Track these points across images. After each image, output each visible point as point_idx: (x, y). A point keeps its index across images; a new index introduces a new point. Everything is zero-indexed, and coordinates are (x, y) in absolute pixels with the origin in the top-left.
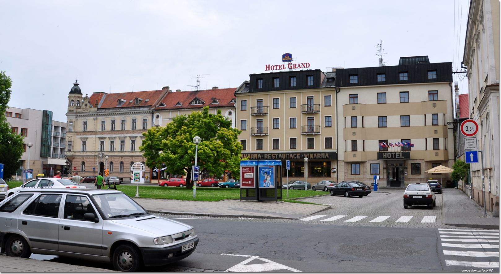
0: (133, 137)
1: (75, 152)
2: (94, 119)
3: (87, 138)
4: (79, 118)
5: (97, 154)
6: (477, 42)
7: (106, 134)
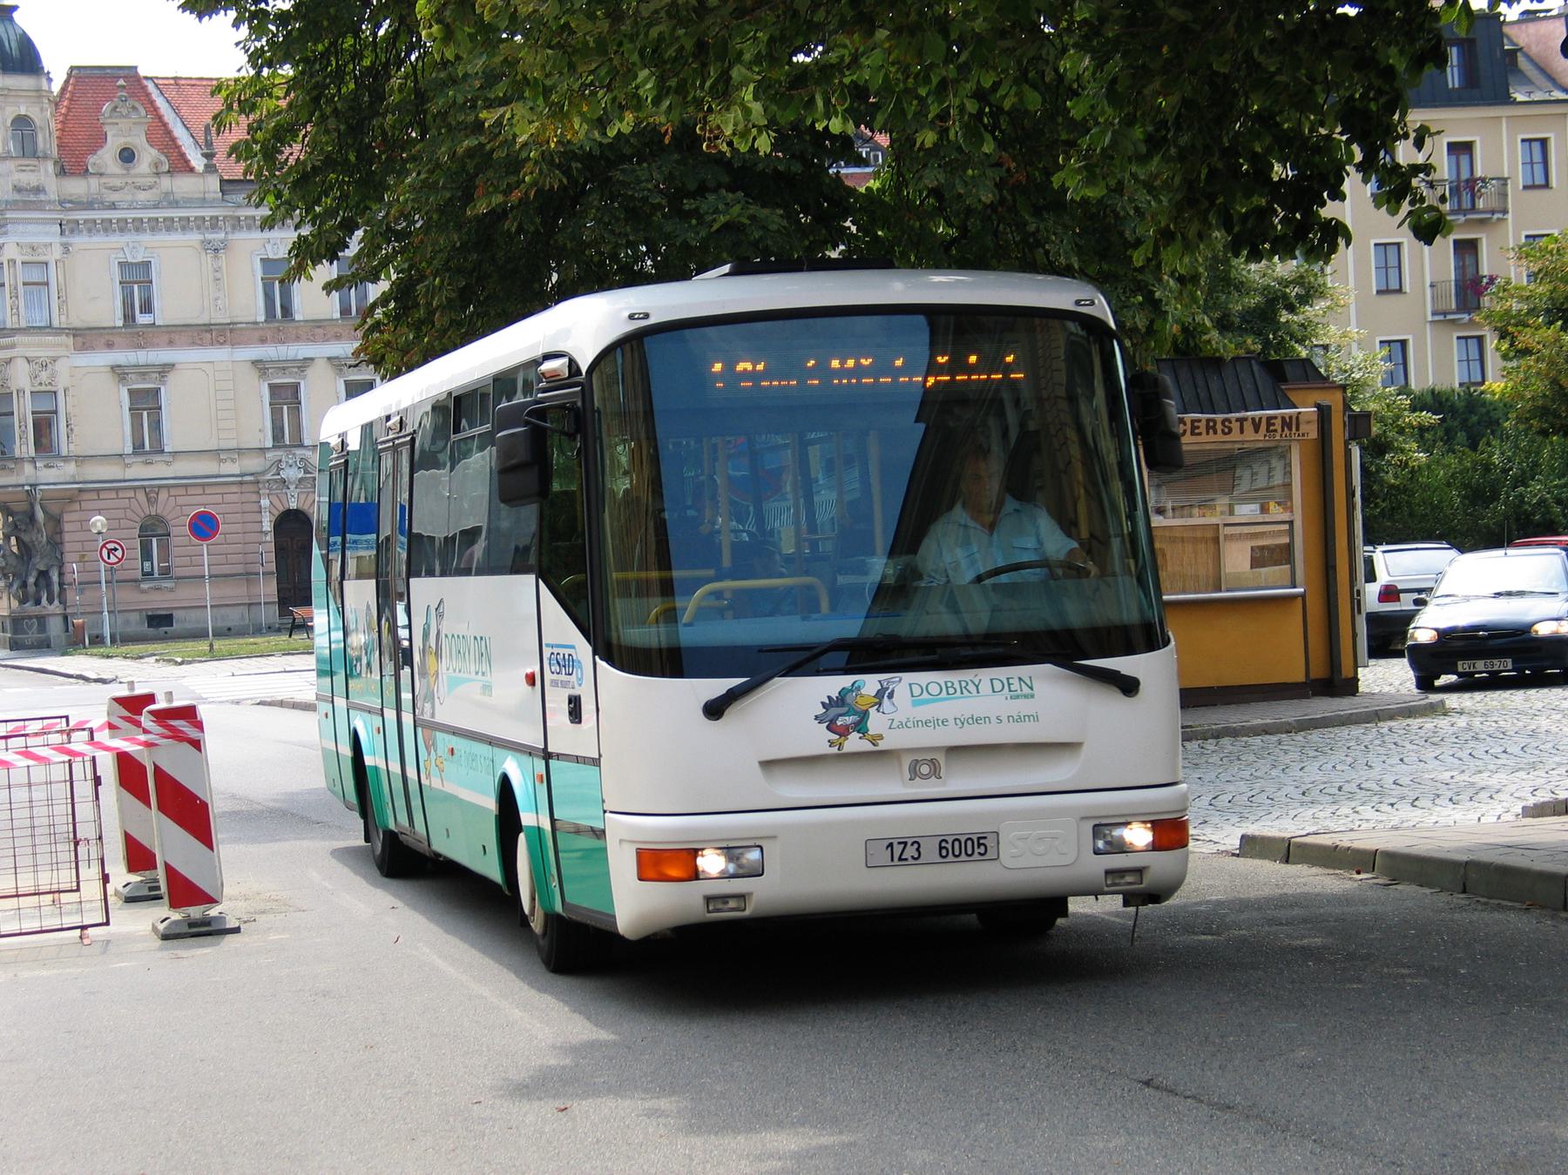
0: (283, 366)
1: (81, 459)
2: (207, 246)
3: (165, 369)
4: (79, 241)
5: (253, 464)
6: (1186, 478)
7: (312, 339)
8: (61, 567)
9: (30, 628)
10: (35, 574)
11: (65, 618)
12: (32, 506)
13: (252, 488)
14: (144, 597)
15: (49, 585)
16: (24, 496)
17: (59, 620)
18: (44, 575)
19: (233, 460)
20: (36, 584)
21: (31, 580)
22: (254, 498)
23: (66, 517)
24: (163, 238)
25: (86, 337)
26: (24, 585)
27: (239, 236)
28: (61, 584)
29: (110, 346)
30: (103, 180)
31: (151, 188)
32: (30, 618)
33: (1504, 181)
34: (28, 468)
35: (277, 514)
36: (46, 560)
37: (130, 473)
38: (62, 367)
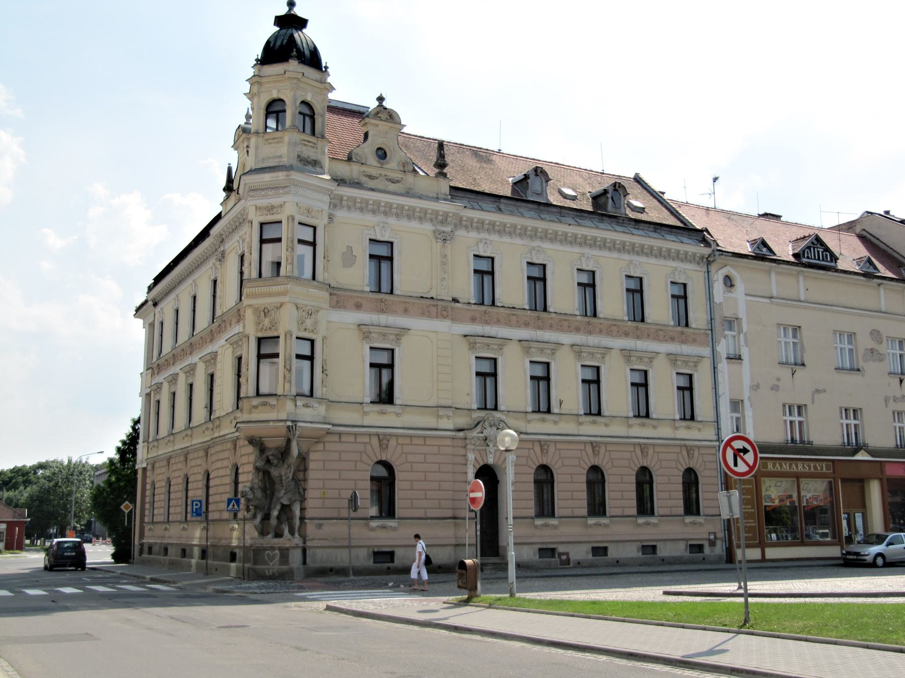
8: (303, 500)
9: (271, 559)
10: (279, 507)
11: (304, 551)
12: (289, 441)
13: (461, 443)
15: (290, 520)
18: (286, 509)
19: (448, 417)
20: (278, 518)
21: (275, 513)
22: (462, 452)
23: (312, 456)
24: (404, 223)
25: (339, 297)
26: (267, 517)
27: (461, 233)
28: (302, 519)
29: (358, 307)
30: (364, 168)
31: (398, 182)
32: (273, 549)
34: (289, 405)
35: (478, 467)
36: (290, 495)
38: (323, 316)
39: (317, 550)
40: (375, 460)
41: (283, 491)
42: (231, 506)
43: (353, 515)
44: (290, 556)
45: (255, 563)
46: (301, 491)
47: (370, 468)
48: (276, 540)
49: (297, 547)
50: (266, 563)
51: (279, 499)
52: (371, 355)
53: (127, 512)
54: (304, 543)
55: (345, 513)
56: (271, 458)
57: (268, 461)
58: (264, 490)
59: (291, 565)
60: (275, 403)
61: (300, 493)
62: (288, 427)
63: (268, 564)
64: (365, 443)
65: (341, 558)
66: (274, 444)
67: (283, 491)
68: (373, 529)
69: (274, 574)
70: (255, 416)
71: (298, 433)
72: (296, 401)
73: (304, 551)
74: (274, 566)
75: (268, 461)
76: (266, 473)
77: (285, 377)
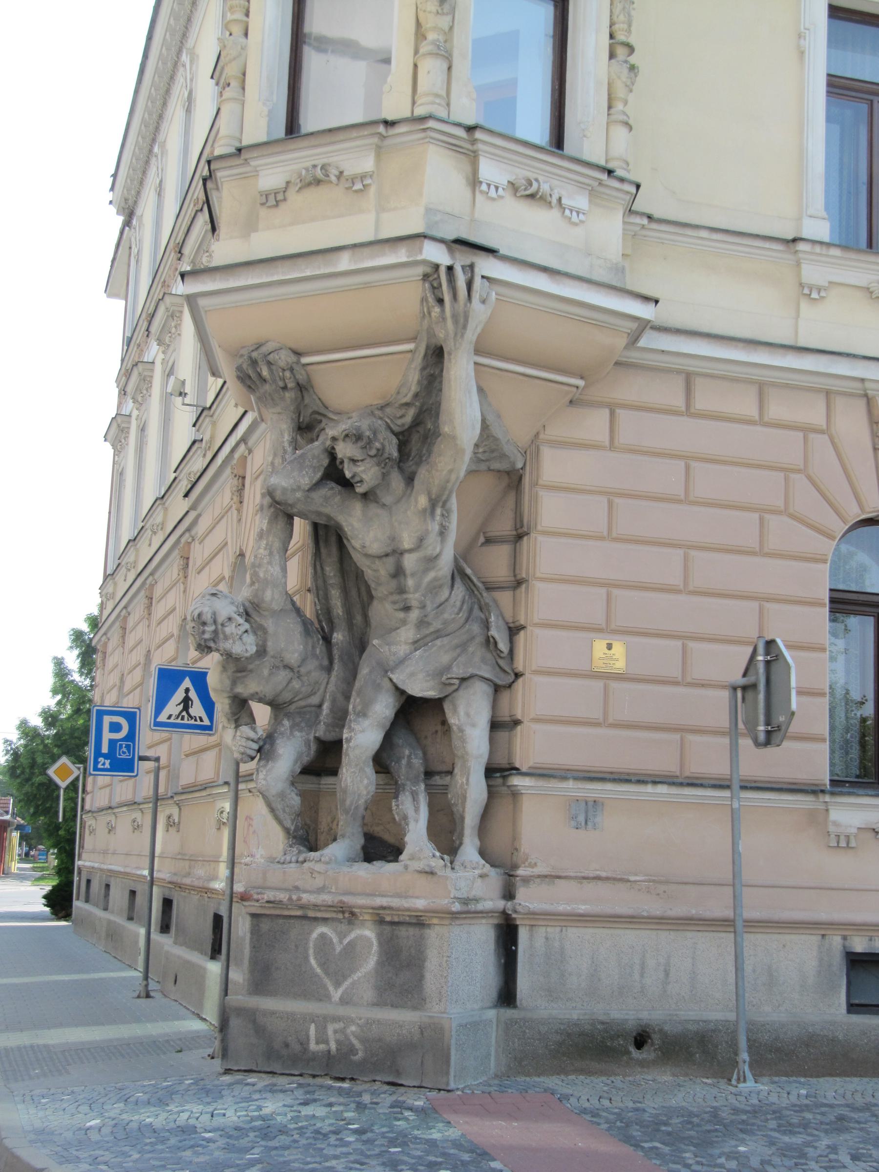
9: (339, 966)
10: (384, 708)
11: (507, 934)
14: (839, 867)
15: (436, 776)
16: (410, 296)
17: (481, 938)
20: (382, 761)
21: (364, 737)
23: (553, 467)
26: (325, 759)
28: (497, 772)
32: (348, 915)
33: (131, 717)
36: (441, 654)
37: (818, 325)
39: (573, 933)
40: (855, 514)
41: (407, 634)
42: (173, 707)
43: (756, 762)
44: (432, 963)
45: (262, 979)
46: (499, 634)
47: (828, 547)
48: (364, 871)
49: (466, 913)
50: (306, 988)
51: (385, 670)
52: (833, 41)
53: (63, 784)
54: (509, 894)
55: (710, 757)
56: (344, 450)
57: (334, 474)
58: (321, 630)
59: (434, 1010)
60: (367, 164)
61: (490, 643)
62: (432, 274)
63: (323, 997)
64: (807, 430)
65: (690, 980)
66: (361, 389)
67: (407, 634)
68: (843, 843)
69: (346, 1051)
70: (268, 241)
71: (479, 312)
72: (473, 158)
73: (507, 934)
74: (347, 1007)
75: (334, 474)
76: (328, 537)
77: (420, 33)
